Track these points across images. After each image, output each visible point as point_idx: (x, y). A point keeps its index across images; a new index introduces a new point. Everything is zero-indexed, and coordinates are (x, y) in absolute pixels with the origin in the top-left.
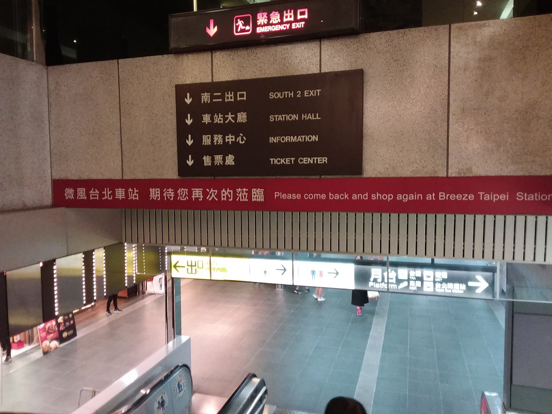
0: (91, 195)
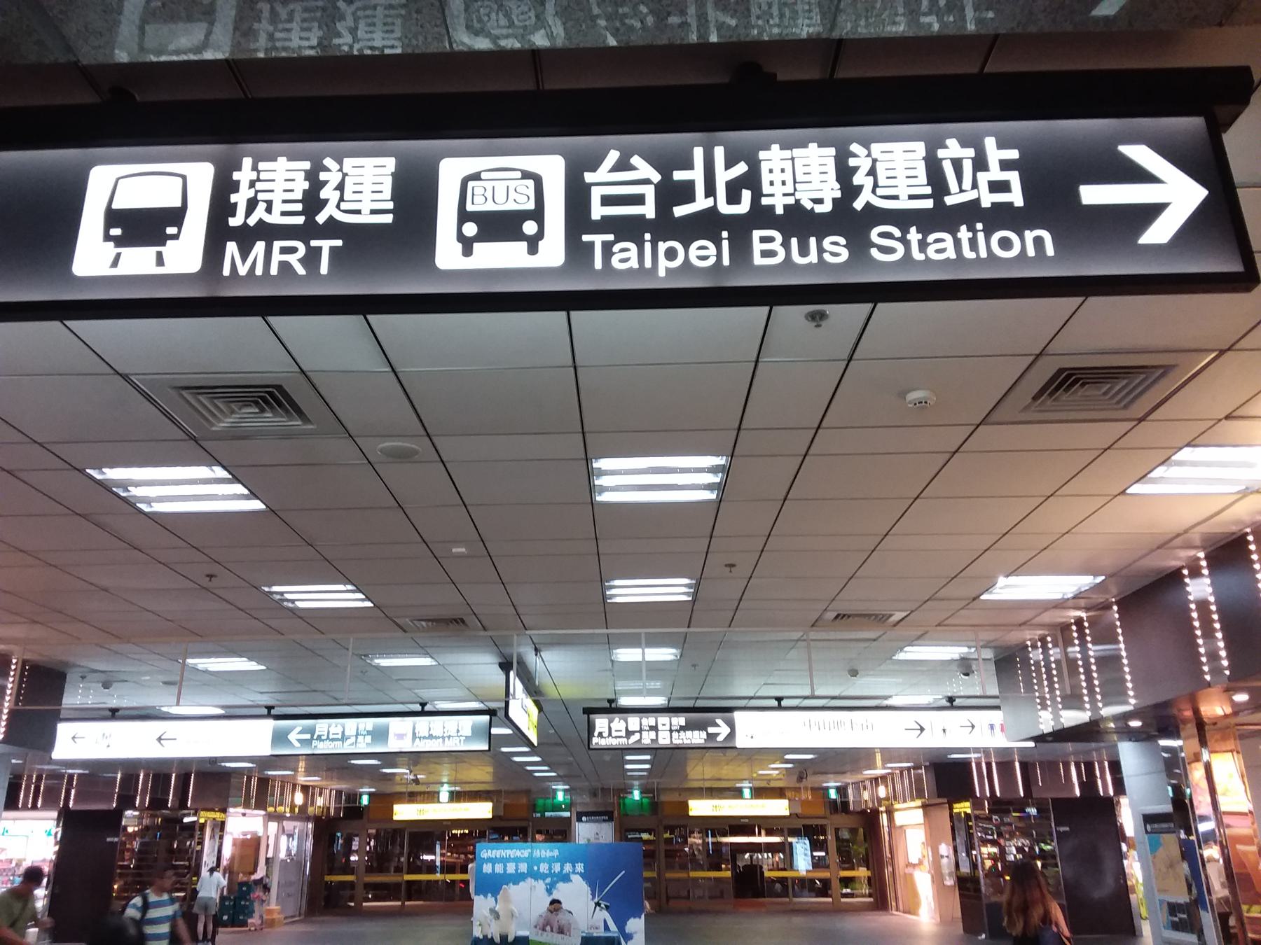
0: (596, 194)
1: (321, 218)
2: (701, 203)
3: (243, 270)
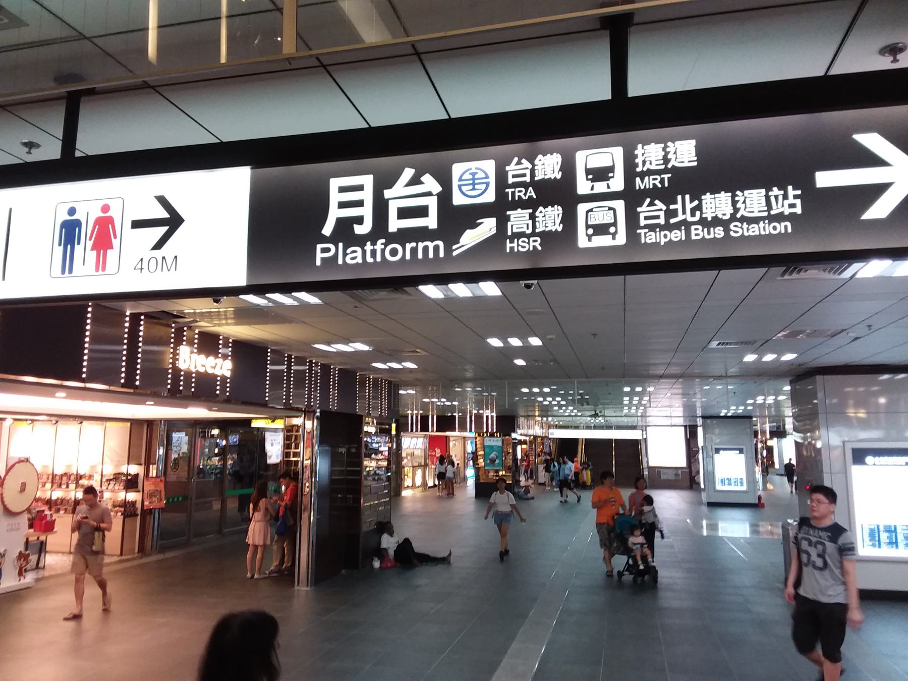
0: (642, 216)
1: (669, 166)
2: (681, 217)
3: (642, 187)
